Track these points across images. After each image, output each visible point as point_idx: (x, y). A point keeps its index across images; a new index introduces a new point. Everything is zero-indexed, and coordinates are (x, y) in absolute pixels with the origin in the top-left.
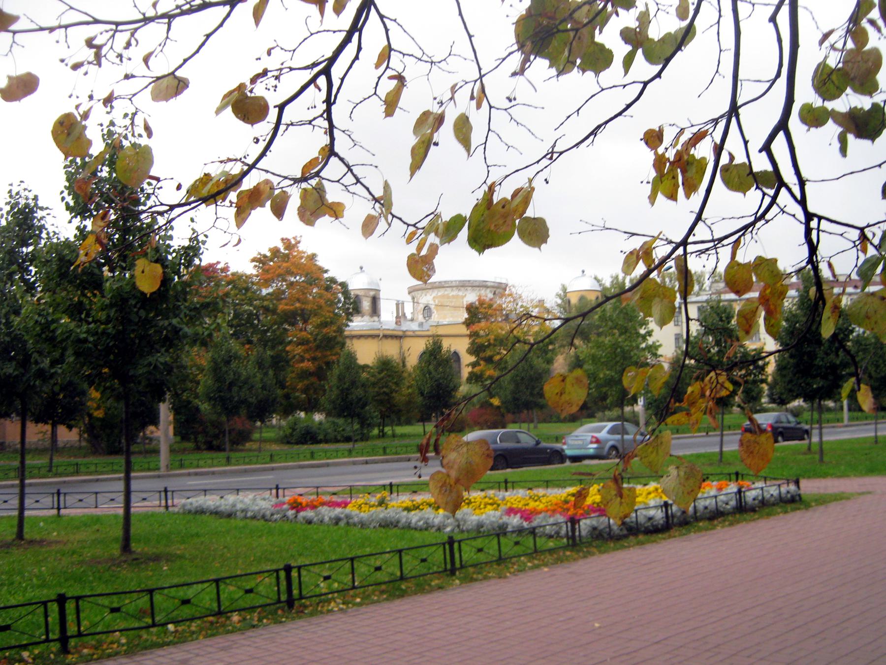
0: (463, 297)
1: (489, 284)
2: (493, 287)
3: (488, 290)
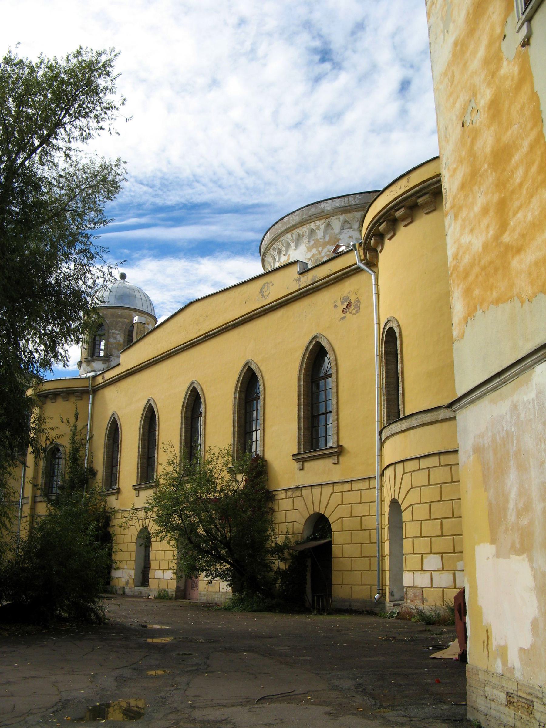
1: (328, 207)
2: (344, 210)
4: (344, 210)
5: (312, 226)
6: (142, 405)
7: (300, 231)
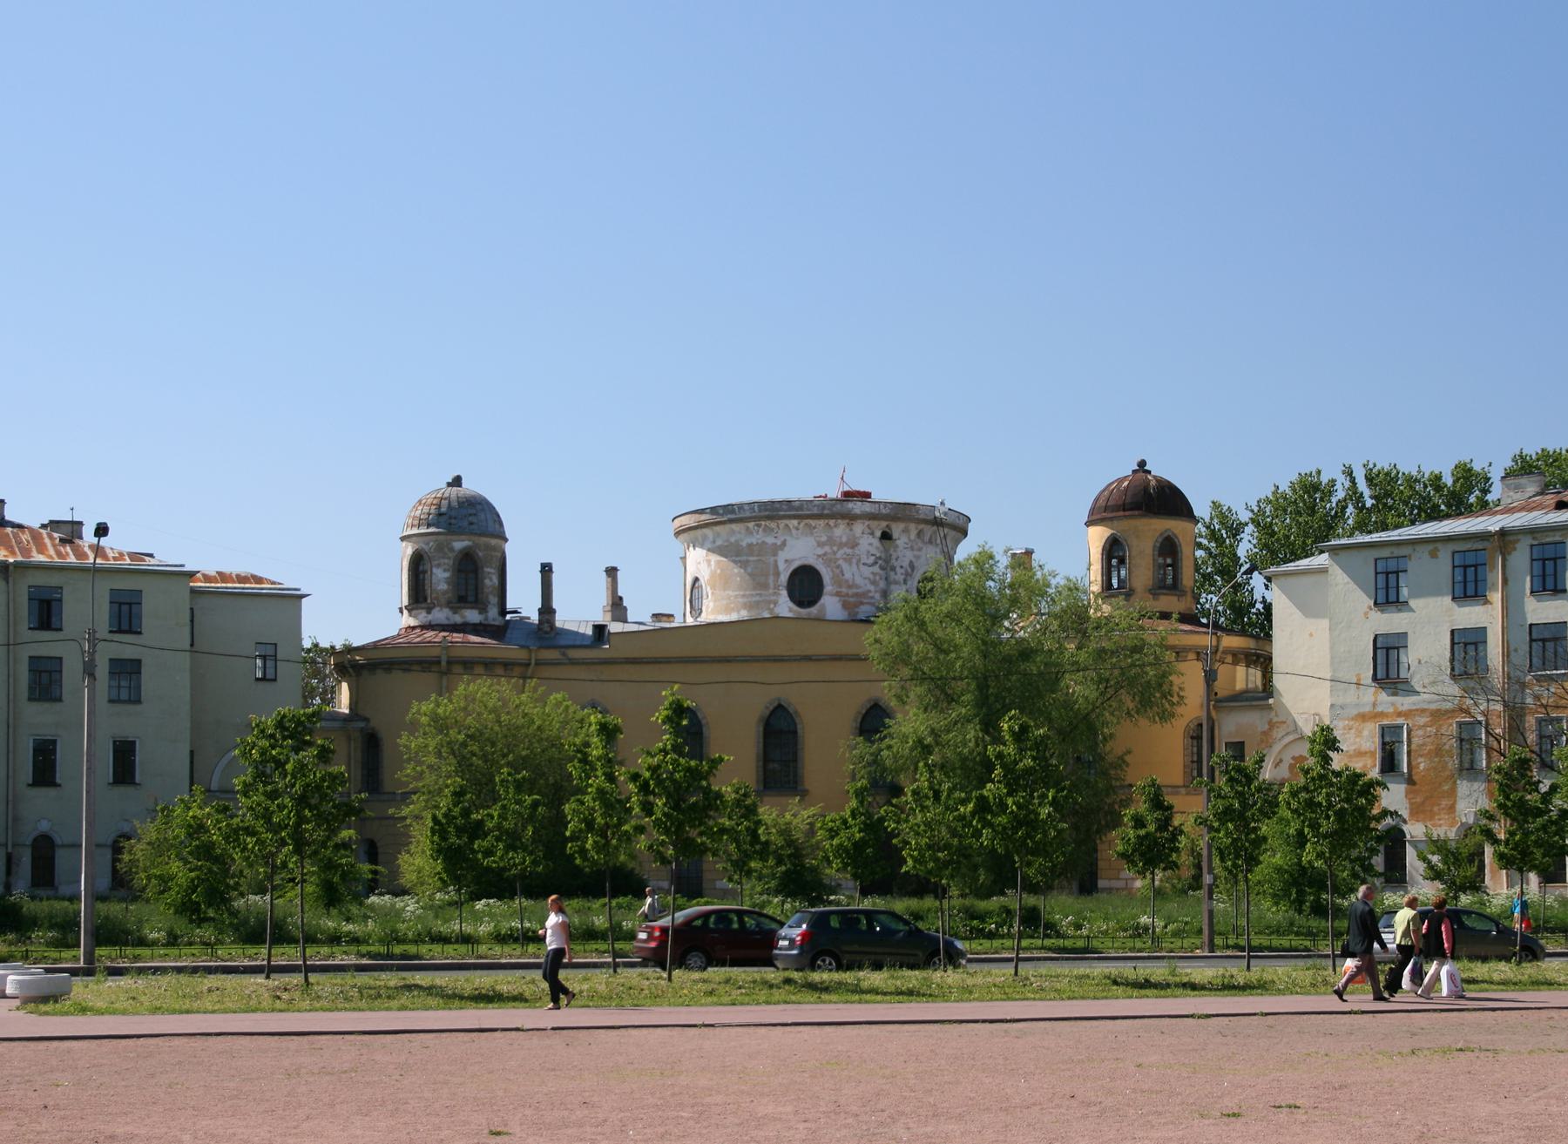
0: (776, 549)
3: (859, 527)
5: (832, 522)
6: (433, 484)
7: (813, 523)
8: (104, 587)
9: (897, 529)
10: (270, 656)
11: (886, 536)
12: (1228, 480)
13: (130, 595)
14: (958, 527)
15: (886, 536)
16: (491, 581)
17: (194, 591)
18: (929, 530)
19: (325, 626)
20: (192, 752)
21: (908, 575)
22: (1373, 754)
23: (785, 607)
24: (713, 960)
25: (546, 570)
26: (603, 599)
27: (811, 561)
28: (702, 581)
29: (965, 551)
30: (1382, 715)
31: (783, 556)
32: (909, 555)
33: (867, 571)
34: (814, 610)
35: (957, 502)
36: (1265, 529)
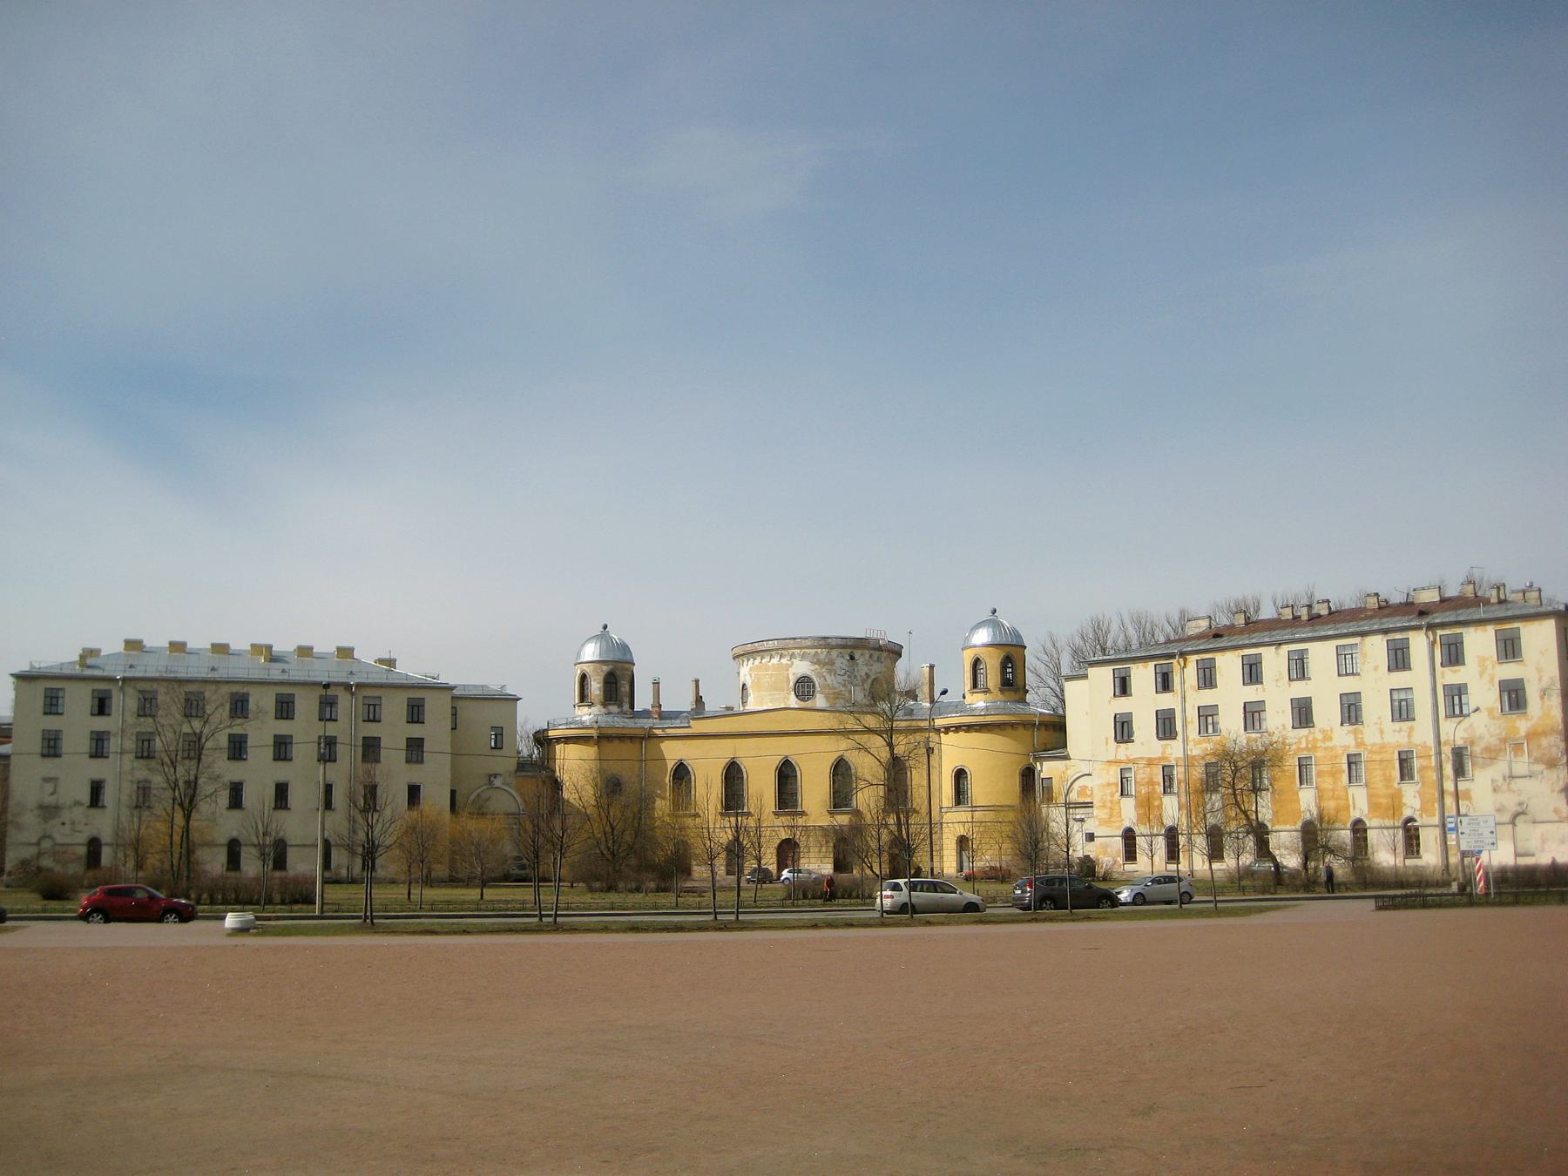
0: (788, 667)
1: (833, 642)
2: (844, 647)
4: (844, 647)
8: (181, 692)
9: (857, 654)
10: (499, 733)
11: (852, 658)
12: (1046, 627)
13: (417, 700)
14: (895, 652)
15: (852, 658)
16: (625, 688)
17: (454, 698)
18: (876, 654)
19: (529, 718)
20: (453, 793)
21: (864, 681)
22: (1553, 731)
23: (793, 702)
24: (1126, 845)
25: (656, 684)
26: (691, 698)
27: (809, 673)
28: (749, 685)
29: (901, 665)
30: (1120, 762)
31: (791, 671)
32: (865, 669)
33: (840, 679)
34: (809, 704)
35: (893, 636)
36: (1076, 652)
